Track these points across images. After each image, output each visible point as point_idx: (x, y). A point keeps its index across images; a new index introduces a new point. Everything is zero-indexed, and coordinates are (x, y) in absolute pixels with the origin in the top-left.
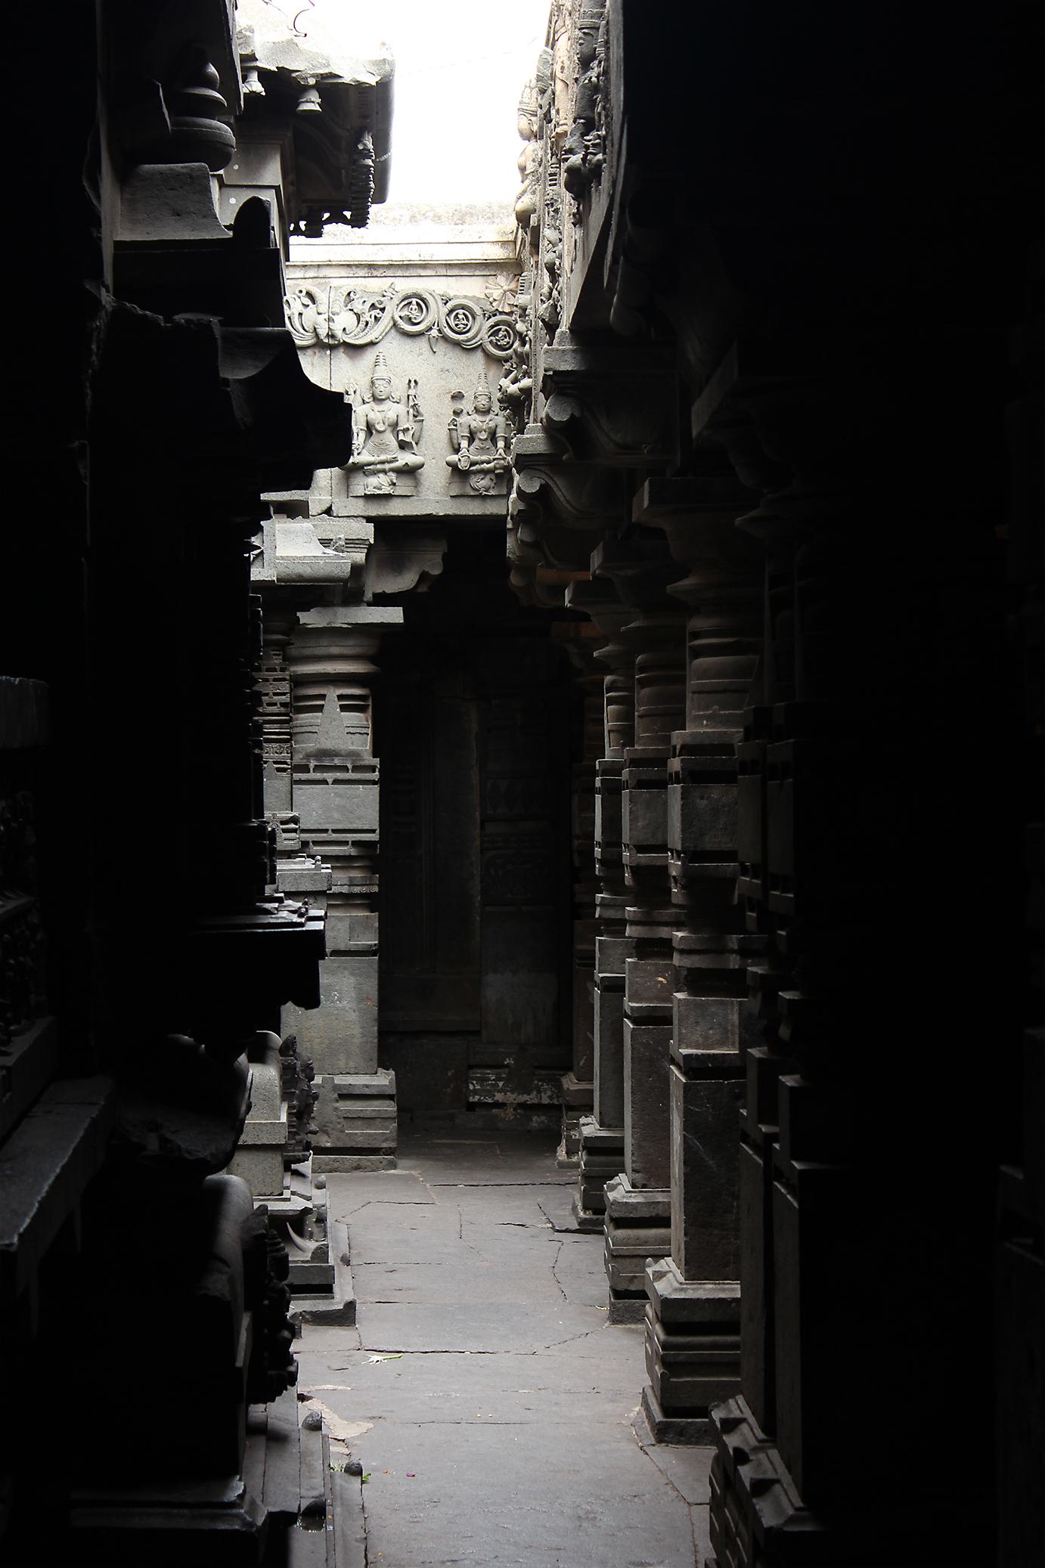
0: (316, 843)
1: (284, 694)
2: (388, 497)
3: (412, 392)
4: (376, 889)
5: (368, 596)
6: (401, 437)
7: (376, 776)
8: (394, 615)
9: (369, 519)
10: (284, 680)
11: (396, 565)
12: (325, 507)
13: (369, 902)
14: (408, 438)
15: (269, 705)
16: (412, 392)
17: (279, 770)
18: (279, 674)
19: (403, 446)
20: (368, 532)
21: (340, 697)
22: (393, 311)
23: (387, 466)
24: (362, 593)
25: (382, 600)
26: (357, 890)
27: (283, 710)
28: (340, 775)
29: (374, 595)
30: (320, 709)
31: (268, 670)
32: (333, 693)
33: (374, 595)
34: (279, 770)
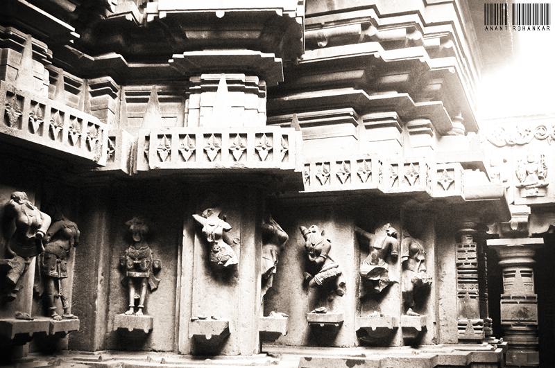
0: (514, 325)
1: (474, 258)
2: (535, 197)
3: (543, 159)
4: (537, 343)
5: (530, 235)
6: (539, 175)
7: (536, 301)
8: (541, 241)
9: (528, 205)
10: (474, 251)
11: (541, 223)
12: (512, 202)
13: (536, 348)
14: (541, 175)
15: (466, 264)
16: (543, 159)
17: (471, 297)
18: (470, 249)
19: (540, 178)
20: (528, 210)
21: (228, 82)
22: (534, 132)
23: (534, 186)
24: (528, 233)
25: (535, 236)
26: (530, 343)
27: (473, 267)
28: (522, 300)
29: (533, 234)
30: (514, 276)
31: (465, 246)
32: (518, 270)
33: (533, 234)
34: (471, 297)
